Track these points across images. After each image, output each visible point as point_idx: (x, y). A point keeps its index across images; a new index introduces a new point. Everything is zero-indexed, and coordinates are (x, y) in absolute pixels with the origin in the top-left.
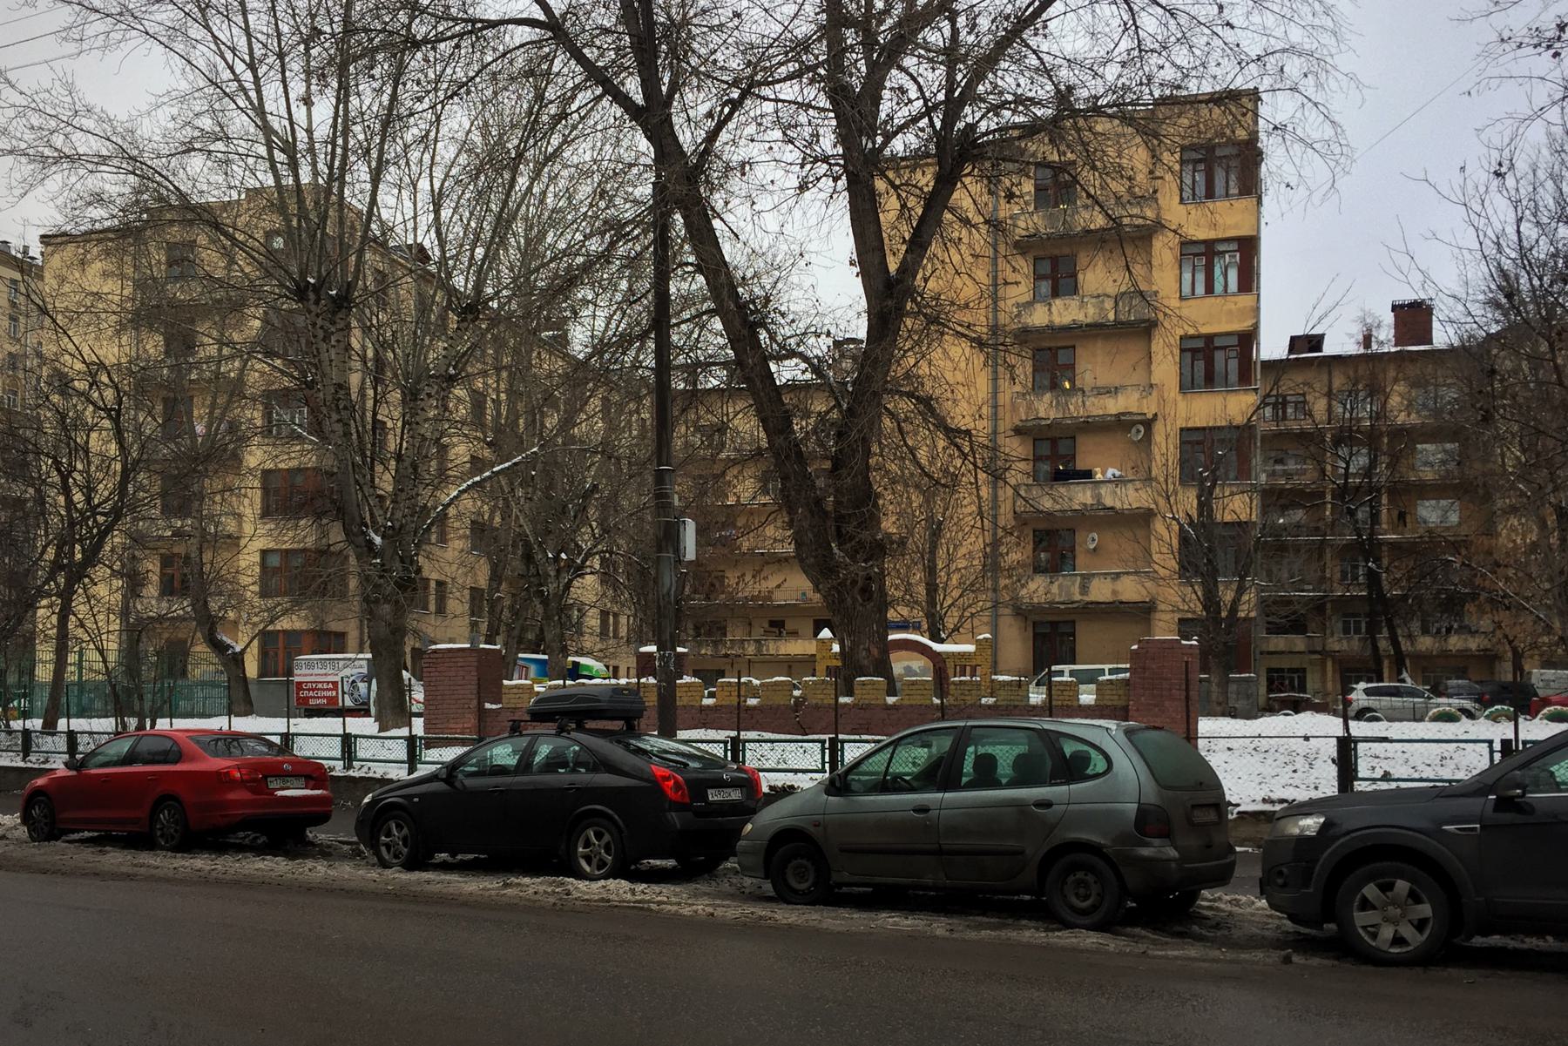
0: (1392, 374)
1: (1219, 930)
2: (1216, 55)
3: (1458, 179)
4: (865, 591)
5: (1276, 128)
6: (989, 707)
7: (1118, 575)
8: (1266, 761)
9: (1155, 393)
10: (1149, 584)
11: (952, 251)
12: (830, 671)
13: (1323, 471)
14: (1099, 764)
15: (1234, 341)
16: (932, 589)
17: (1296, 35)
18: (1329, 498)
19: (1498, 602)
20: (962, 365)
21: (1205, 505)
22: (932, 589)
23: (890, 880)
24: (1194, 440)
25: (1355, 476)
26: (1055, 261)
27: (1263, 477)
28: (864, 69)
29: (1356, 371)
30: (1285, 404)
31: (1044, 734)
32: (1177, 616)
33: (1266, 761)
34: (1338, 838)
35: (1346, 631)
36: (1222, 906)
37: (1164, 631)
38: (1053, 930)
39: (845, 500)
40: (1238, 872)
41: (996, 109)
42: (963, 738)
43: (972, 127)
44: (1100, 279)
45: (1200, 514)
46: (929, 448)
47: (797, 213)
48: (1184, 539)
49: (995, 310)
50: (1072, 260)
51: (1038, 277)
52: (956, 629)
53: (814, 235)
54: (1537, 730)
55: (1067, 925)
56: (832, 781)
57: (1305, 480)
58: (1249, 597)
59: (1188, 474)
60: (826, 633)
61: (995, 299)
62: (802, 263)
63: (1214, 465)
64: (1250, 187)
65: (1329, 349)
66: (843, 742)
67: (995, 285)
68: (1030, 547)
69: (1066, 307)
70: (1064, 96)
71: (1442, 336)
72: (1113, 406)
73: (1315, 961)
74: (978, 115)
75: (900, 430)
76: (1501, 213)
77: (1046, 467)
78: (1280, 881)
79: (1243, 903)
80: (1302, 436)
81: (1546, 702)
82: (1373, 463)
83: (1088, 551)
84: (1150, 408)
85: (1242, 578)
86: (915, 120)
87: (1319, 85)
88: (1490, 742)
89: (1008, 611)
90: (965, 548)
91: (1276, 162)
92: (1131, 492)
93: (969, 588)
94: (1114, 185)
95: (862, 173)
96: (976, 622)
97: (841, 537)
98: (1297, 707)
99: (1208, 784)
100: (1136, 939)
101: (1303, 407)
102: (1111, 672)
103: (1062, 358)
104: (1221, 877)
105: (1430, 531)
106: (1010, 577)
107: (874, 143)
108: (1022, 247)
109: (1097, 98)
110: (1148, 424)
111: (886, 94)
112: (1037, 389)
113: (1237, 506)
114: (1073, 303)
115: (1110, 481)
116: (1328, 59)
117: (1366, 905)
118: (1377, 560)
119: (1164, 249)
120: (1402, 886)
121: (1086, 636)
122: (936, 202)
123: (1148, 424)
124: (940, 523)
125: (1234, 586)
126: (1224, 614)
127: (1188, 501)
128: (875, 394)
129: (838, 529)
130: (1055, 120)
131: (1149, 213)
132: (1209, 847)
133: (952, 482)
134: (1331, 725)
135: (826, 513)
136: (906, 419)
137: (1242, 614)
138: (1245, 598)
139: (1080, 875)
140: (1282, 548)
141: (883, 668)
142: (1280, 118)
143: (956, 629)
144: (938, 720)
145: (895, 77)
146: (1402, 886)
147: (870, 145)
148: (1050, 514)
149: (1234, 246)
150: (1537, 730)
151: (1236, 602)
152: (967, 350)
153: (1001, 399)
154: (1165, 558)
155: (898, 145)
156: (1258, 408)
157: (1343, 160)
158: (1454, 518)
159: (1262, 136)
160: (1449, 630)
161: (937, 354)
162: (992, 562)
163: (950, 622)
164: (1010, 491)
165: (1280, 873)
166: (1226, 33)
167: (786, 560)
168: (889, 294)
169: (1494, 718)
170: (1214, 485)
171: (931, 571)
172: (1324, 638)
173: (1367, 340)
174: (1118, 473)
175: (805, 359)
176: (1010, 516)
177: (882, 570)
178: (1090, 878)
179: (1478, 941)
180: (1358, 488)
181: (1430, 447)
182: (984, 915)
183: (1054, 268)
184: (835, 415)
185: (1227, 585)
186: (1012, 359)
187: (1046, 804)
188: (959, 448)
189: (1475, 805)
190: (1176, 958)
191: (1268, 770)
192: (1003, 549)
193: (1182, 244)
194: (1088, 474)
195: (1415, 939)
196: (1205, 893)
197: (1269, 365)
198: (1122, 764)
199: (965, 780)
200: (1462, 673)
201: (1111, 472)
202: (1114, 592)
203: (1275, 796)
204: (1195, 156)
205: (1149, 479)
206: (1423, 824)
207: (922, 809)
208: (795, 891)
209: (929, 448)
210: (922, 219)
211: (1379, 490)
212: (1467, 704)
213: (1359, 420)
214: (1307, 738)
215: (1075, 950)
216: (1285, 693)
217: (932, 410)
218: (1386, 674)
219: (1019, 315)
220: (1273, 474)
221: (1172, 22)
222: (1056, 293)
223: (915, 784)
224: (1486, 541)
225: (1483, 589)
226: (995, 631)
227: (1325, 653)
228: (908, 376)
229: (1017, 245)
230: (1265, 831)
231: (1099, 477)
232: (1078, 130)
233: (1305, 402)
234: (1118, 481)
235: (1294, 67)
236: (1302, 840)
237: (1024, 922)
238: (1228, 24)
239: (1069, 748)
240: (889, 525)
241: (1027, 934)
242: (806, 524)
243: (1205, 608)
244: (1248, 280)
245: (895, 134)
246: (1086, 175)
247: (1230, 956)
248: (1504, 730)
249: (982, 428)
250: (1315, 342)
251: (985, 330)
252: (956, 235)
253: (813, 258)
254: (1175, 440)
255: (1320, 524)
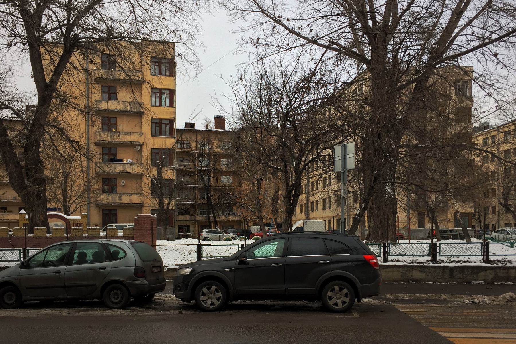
0: (214, 137)
1: (161, 306)
2: (160, 27)
3: (230, 78)
4: (38, 196)
5: (179, 55)
6: (85, 237)
7: (131, 194)
8: (176, 253)
9: (143, 136)
10: (141, 198)
11: (71, 78)
12: (24, 225)
13: (195, 165)
14: (121, 254)
15: (168, 122)
16: (65, 197)
17: (185, 27)
18: (196, 173)
19: (242, 206)
20: (75, 119)
21: (159, 173)
22: (65, 197)
23: (46, 298)
24: (156, 152)
25: (204, 167)
26: (109, 87)
27: (177, 166)
28: (35, 5)
29: (204, 135)
30: (184, 143)
31: (104, 245)
32: (151, 208)
33: (176, 253)
34: (196, 274)
35: (201, 214)
36: (162, 298)
37: (146, 212)
38: (106, 310)
39: (29, 162)
40: (167, 287)
41: (85, 30)
42: (74, 247)
43: (77, 35)
44: (124, 95)
45: (158, 176)
46: (63, 147)
47: (8, 55)
48: (153, 183)
49: (88, 100)
50: (115, 88)
51: (103, 92)
52: (74, 211)
53: (15, 64)
54: (249, 242)
55: (111, 308)
56: (22, 263)
57: (188, 168)
58: (173, 203)
59: (154, 163)
60: (23, 211)
61: (88, 97)
62: (10, 73)
63: (162, 160)
64: (172, 73)
65: (196, 128)
66: (28, 250)
67: (88, 93)
68: (101, 184)
69: (113, 104)
70: (110, 30)
71: (228, 127)
72: (130, 139)
73: (189, 312)
74: (79, 31)
75: (51, 139)
76: (242, 91)
77: (107, 157)
78: (179, 289)
79: (168, 297)
80: (188, 154)
81: (254, 235)
82: (209, 163)
83: (121, 186)
84: (142, 140)
85: (171, 196)
86: (55, 29)
87: (192, 44)
88: (238, 245)
89: (93, 205)
90: (77, 183)
91: (180, 66)
92: (136, 167)
93: (79, 197)
94: (128, 65)
95: (35, 44)
96: (82, 209)
97: (29, 177)
98: (187, 237)
99: (158, 260)
100: (134, 310)
101: (189, 144)
102: (129, 225)
103: (112, 121)
104: (161, 289)
105: (224, 185)
106: (94, 193)
107: (39, 34)
108: (98, 81)
109: (121, 34)
110: (141, 146)
111: (43, 16)
112: (103, 130)
113: (169, 174)
114: (116, 102)
115: (128, 163)
116: (195, 36)
117: (203, 294)
118: (210, 193)
119: (145, 89)
120: (213, 288)
121: (121, 214)
122: (64, 59)
123: (141, 146)
124: (68, 174)
125: (168, 199)
126: (165, 208)
127: (154, 171)
128: (41, 125)
129: (27, 173)
130: (107, 38)
131: (140, 76)
132: (157, 279)
133: (72, 160)
134: (196, 241)
135: (22, 167)
136: (54, 135)
137: (171, 208)
138: (171, 203)
139: (115, 291)
140: (183, 188)
141: (45, 224)
142: (180, 52)
143: (74, 211)
144: (66, 241)
145: (47, 11)
146: (213, 288)
147: (38, 34)
148: (108, 173)
149: (168, 92)
150: (249, 242)
151: (169, 204)
152: (77, 114)
153: (90, 132)
154: (147, 190)
155: (49, 36)
156: (176, 143)
157: (199, 68)
158: (231, 181)
159: (175, 57)
160: (229, 214)
161: (65, 113)
162: (88, 189)
163: (72, 209)
164: (94, 165)
165: (179, 286)
166: (163, 21)
167: (7, 185)
168: (46, 90)
169: (241, 240)
170: (162, 167)
171: (65, 190)
172: (195, 216)
173: (207, 126)
174: (131, 161)
175: (12, 109)
176: (94, 172)
177: (45, 189)
178: (119, 292)
179: (234, 303)
180: (204, 171)
181: (225, 160)
182: (81, 307)
183: (109, 90)
184: (25, 131)
185: (166, 199)
186: (94, 118)
187: (104, 268)
188: (75, 148)
189: (233, 263)
190: (146, 315)
191: (177, 255)
192: (92, 184)
193: (152, 88)
194: (121, 161)
195: (217, 303)
196: (157, 294)
197: (179, 131)
198: (130, 255)
199: (74, 262)
200: (232, 227)
201: (129, 160)
202: (130, 200)
203: (178, 263)
204: (156, 60)
205: (142, 164)
206: (220, 269)
207: (59, 272)
208: (8, 304)
209: (63, 147)
210: (59, 64)
211: (210, 172)
212: (234, 236)
213: (205, 150)
214: (188, 245)
215: (113, 316)
216: (184, 233)
217: (64, 133)
218: (212, 227)
219: (96, 104)
220: (180, 165)
221: (146, 13)
222: (110, 99)
223: (55, 263)
224: (239, 188)
225: (238, 202)
226: (89, 211)
227: (195, 220)
228: (54, 120)
229: (95, 80)
230: (175, 274)
231: (125, 162)
232: (116, 43)
233: (189, 143)
234: (131, 164)
235: (184, 36)
236: (186, 276)
237: (96, 308)
238: (164, 18)
239: (112, 250)
240: (47, 173)
241: (96, 312)
242: (13, 171)
243: (159, 206)
244: (172, 103)
245: (48, 32)
246: (119, 60)
247: (163, 313)
248: (243, 242)
249: (83, 142)
250: (192, 125)
251: (83, 107)
252: (72, 72)
253: (15, 72)
254: (150, 152)
255: (194, 181)
